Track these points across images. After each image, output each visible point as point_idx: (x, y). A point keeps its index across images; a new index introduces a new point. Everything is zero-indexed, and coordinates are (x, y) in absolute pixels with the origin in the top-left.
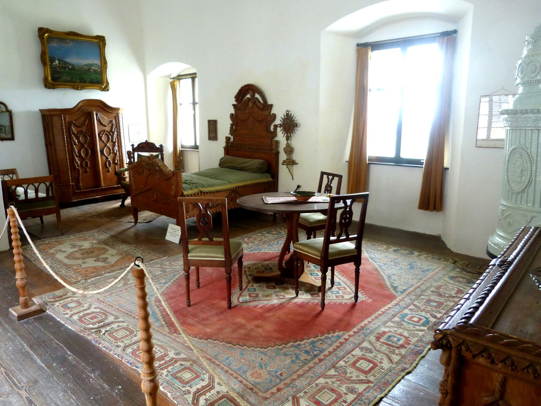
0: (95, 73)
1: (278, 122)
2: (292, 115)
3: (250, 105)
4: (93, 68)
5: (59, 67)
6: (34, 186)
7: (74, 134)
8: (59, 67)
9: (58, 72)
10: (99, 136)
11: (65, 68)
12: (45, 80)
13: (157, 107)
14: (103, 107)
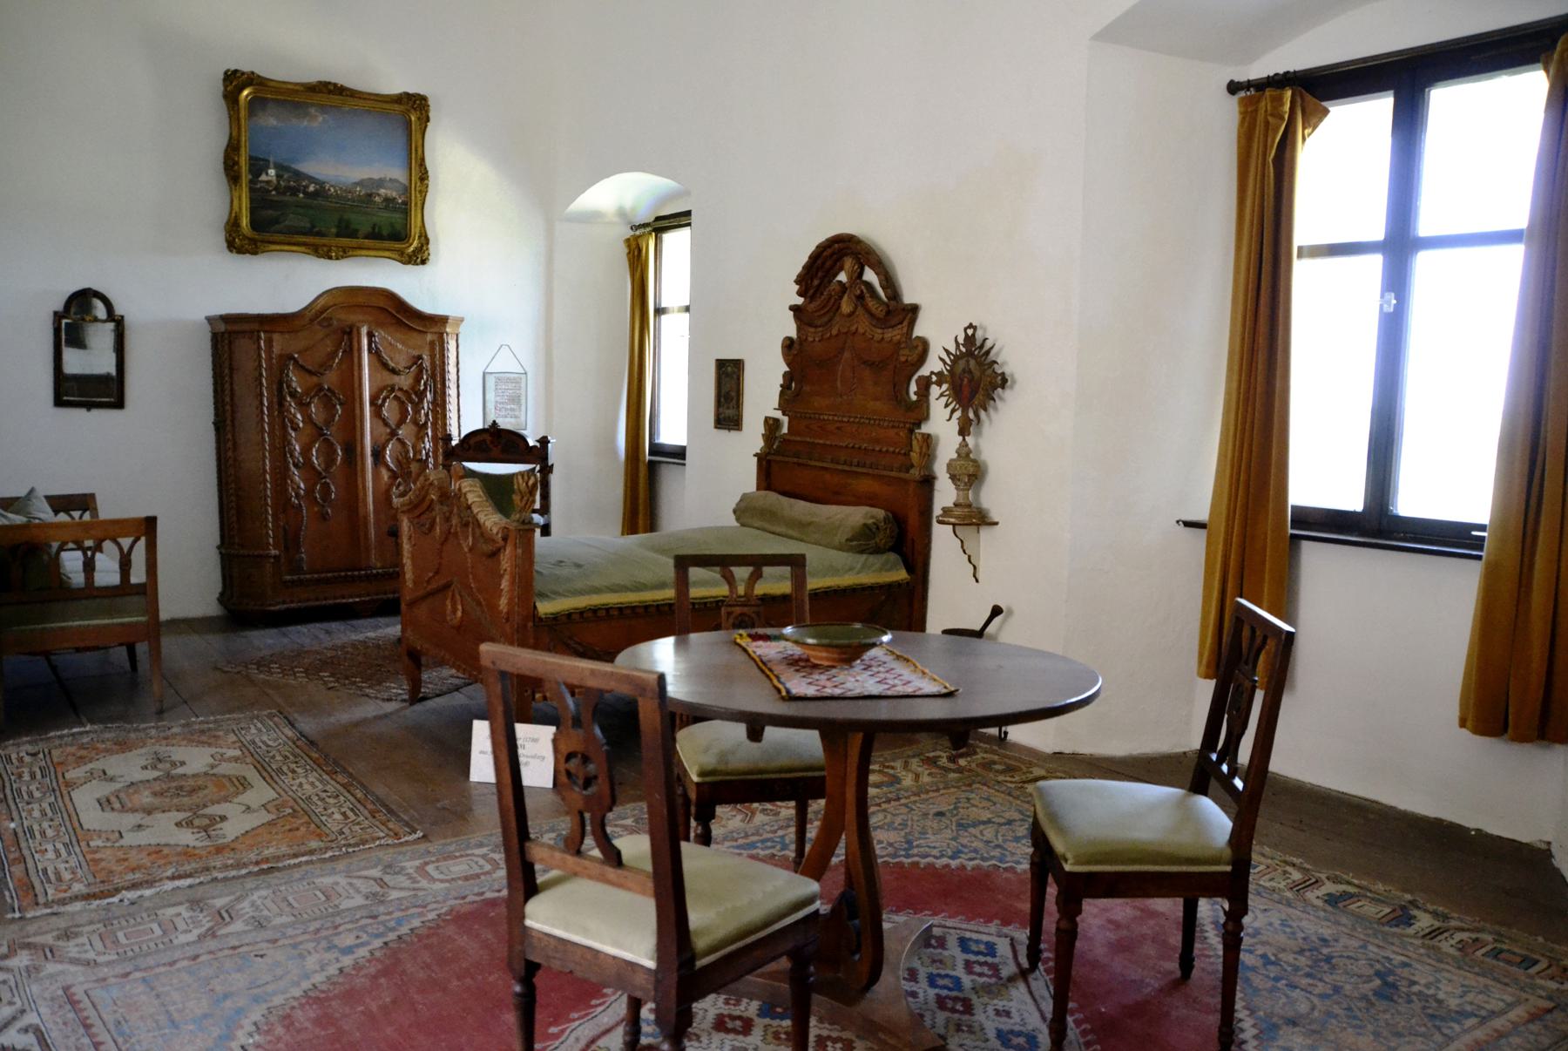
0: (386, 208)
1: (933, 365)
2: (988, 344)
3: (846, 307)
4: (382, 191)
5: (276, 189)
6: (121, 549)
7: (293, 394)
8: (276, 189)
9: (273, 205)
10: (372, 403)
11: (294, 191)
12: (232, 226)
13: (553, 312)
14: (395, 312)
